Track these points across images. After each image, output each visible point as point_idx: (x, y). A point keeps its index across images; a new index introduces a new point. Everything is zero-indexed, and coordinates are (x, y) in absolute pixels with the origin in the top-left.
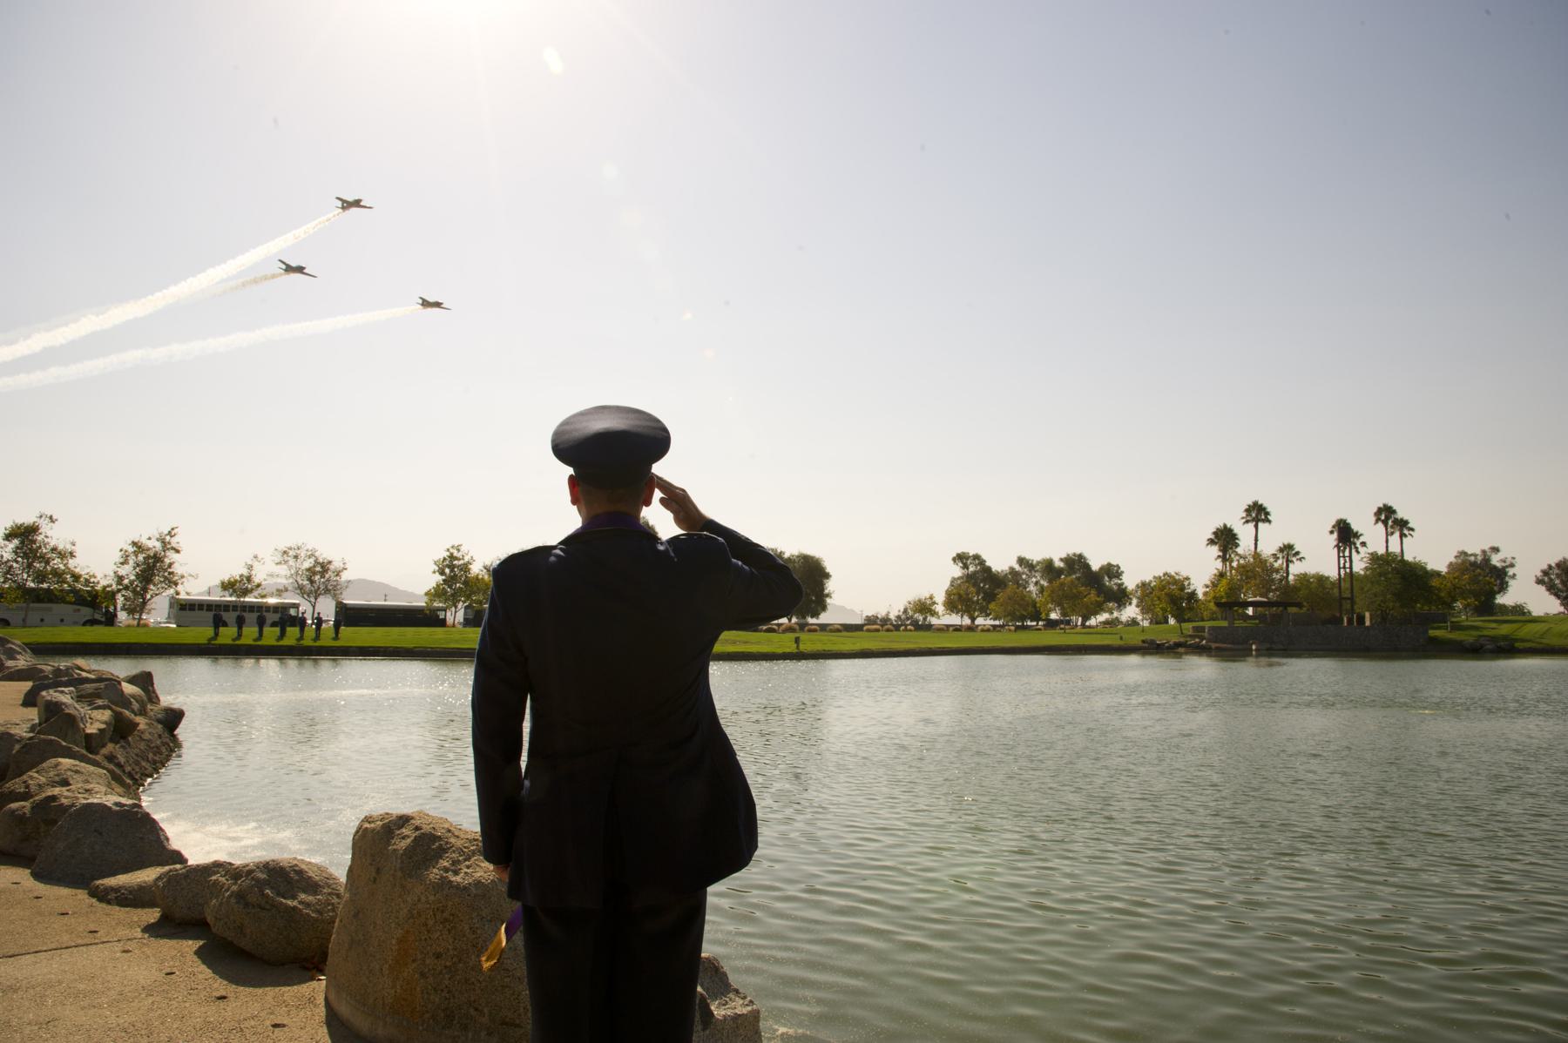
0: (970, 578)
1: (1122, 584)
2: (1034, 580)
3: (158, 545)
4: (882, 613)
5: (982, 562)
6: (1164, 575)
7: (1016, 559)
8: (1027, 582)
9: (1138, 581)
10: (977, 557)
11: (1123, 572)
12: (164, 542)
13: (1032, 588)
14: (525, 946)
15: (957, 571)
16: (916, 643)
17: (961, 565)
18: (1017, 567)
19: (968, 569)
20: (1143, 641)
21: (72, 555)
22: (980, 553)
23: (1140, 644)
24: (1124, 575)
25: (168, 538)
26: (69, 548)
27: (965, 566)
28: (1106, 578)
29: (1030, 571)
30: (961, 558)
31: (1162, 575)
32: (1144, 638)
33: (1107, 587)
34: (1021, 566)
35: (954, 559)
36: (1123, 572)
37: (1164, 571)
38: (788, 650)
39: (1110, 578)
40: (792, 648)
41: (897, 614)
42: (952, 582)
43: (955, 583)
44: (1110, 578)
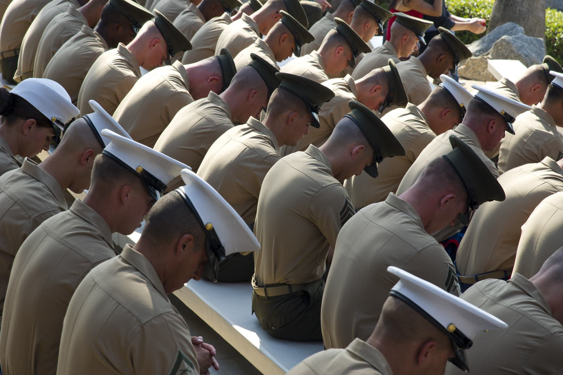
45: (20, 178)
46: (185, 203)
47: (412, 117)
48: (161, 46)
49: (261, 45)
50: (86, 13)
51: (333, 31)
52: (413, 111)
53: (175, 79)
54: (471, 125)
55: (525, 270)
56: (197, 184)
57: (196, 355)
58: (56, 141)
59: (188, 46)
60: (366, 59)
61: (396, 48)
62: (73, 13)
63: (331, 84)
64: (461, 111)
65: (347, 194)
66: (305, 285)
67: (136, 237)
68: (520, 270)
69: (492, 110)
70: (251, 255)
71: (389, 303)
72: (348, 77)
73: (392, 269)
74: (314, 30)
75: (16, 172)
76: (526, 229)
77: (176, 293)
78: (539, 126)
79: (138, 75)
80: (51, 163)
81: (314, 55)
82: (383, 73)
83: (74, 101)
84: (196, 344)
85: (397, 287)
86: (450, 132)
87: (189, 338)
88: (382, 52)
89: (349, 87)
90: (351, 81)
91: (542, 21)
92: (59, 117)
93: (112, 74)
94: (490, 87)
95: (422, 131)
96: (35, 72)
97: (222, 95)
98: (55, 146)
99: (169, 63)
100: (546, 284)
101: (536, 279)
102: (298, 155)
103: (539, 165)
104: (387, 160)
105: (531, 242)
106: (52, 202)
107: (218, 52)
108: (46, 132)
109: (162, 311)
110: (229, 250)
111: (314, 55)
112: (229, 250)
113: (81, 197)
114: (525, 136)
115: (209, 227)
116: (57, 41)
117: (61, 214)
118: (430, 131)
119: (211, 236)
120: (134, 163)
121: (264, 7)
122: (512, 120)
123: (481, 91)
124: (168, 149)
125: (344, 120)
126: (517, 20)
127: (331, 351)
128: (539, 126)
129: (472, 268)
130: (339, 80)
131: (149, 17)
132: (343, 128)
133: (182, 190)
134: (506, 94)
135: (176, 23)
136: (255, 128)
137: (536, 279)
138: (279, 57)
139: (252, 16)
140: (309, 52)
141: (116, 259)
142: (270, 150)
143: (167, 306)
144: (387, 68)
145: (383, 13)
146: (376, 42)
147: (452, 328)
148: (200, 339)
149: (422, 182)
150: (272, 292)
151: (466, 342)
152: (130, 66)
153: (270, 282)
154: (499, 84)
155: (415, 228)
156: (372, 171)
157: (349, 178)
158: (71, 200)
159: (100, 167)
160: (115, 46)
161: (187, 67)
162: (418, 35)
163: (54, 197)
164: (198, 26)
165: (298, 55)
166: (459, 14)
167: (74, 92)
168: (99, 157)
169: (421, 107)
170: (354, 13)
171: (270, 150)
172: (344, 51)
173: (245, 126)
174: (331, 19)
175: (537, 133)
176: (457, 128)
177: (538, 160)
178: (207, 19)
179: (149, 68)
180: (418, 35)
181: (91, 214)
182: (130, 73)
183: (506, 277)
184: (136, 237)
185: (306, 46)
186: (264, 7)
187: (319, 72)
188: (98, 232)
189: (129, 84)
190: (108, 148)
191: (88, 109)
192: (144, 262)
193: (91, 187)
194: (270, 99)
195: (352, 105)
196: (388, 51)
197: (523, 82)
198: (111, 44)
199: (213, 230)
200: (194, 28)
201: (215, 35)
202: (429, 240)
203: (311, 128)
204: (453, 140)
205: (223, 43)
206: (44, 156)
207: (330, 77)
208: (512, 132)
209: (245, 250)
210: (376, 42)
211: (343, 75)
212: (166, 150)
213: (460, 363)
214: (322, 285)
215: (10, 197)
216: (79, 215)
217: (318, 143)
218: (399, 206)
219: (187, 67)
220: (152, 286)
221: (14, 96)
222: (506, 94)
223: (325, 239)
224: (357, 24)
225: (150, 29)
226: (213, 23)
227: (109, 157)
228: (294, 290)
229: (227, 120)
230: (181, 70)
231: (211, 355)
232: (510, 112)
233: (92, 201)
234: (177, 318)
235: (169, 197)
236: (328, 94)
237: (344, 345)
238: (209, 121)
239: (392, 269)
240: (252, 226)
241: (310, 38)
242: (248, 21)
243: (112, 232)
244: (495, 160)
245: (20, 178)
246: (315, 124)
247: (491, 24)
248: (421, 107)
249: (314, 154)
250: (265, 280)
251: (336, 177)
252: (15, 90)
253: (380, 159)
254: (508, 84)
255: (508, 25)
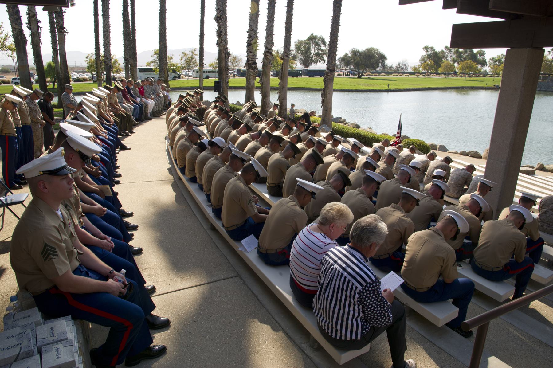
0: (429, 57)
1: (485, 58)
2: (450, 55)
3: (191, 53)
4: (275, 19)
5: (434, 50)
6: (502, 55)
7: (444, 47)
8: (447, 56)
9: (491, 57)
10: (432, 48)
11: (486, 53)
12: (193, 53)
13: (449, 58)
14: (28, 169)
15: (424, 53)
16: (420, 85)
17: (426, 50)
18: (444, 50)
19: (428, 52)
20: (494, 86)
21: (172, 58)
22: (433, 46)
23: (493, 86)
24: (486, 54)
25: (194, 51)
26: (171, 56)
27: (427, 51)
28: (479, 56)
29: (449, 52)
30: (426, 48)
31: (500, 55)
32: (494, 84)
33: (478, 59)
34: (446, 49)
35: (423, 48)
36: (486, 53)
37: (501, 53)
38: (386, 89)
39: (480, 56)
40: (386, 88)
41: (396, 65)
42: (422, 57)
43: (423, 58)
44: (480, 56)
45: (214, 160)
46: (251, 165)
47: (303, 145)
48: (246, 130)
49: (268, 129)
50: (228, 122)
51: (285, 125)
52: (303, 144)
53: (249, 137)
54: (317, 147)
55: (329, 179)
56: (254, 161)
57: (254, 199)
58: (222, 151)
59: (252, 130)
60: (292, 132)
61: (299, 130)
62: (226, 123)
63: (285, 137)
64: (314, 144)
65: (288, 163)
66: (279, 184)
67: (240, 173)
68: (327, 179)
69: (321, 144)
70: (266, 177)
71: (296, 187)
72: (288, 136)
73: (297, 179)
74: (281, 125)
75: (213, 158)
76: (329, 170)
77: (249, 186)
78: (331, 147)
79: (240, 136)
80: (221, 156)
81: (280, 131)
82: (296, 135)
83: (226, 142)
84: (254, 197)
85: (298, 183)
86: (312, 148)
87: (252, 196)
88: (296, 130)
89: (289, 138)
90: (289, 137)
91: (331, 125)
92: (222, 146)
93: (235, 136)
94: (320, 138)
95: (306, 148)
96: (218, 136)
97: (258, 140)
98: (222, 152)
99: (247, 133)
100: (333, 182)
101: (331, 181)
102: (277, 154)
103: (331, 156)
104: (297, 154)
105: (330, 173)
106: (221, 165)
107: (258, 130)
108: (220, 149)
109: (246, 189)
110: (261, 176)
111: (280, 131)
112: (261, 176)
113: (227, 164)
114: (328, 149)
115: (257, 171)
116: (222, 129)
117: (223, 168)
118: (307, 148)
119: (257, 172)
120: (239, 156)
121: (269, 120)
122: (326, 146)
123: (319, 139)
124: (247, 152)
125: (287, 145)
126: (326, 124)
127: (285, 198)
128: (331, 147)
129: (317, 179)
130: (286, 137)
131: (243, 123)
132: (288, 147)
133: (251, 162)
134: (324, 140)
135: (249, 124)
136: (267, 147)
137: (331, 181)
138: (273, 131)
139: (266, 122)
140: (279, 130)
141: (235, 177)
142: (270, 152)
143: (247, 188)
144: (297, 134)
145: (296, 122)
146: (295, 128)
147: (311, 191)
148: (255, 196)
149: (306, 160)
150: (271, 185)
151: (314, 194)
152: (238, 134)
153: (271, 183)
154: (322, 137)
155: (304, 170)
156: (294, 157)
157: (289, 159)
158: (225, 164)
159: (231, 157)
160: (235, 130)
161: (251, 134)
162: (304, 127)
163: (221, 164)
164: (254, 125)
165: (277, 131)
166: (313, 122)
167: (226, 140)
168: (231, 154)
169: (305, 143)
170: (289, 122)
171: (270, 152)
172: (287, 130)
173: (265, 147)
174: (284, 123)
175: (331, 149)
176: (313, 148)
177: (331, 155)
178: (256, 123)
179: (243, 134)
180: (304, 127)
181: (230, 167)
182: (239, 136)
183: (324, 180)
184: (240, 173)
185: (279, 129)
186: (269, 120)
187: (282, 135)
188: (231, 172)
189: (238, 138)
190: (233, 152)
191: (229, 144)
192: (242, 178)
193: (229, 161)
194: (180, 141)
195: (289, 142)
196: (297, 130)
197: (327, 137)
198: (234, 129)
199: (258, 171)
200: (253, 125)
201: (258, 127)
202: (307, 173)
203: (280, 147)
204: (313, 150)
205: (259, 129)
206: (219, 155)
207: (284, 136)
208: (326, 149)
209: (265, 176)
210: (295, 128)
211: (287, 136)
212: (246, 152)
213: (314, 198)
214: (283, 184)
215: (212, 164)
216: (227, 168)
217: (282, 151)
218: (300, 165)
219: (251, 134)
220: (244, 184)
221: (213, 141)
222: (324, 140)
223: (283, 173)
224: (290, 124)
225: (243, 126)
226: (257, 124)
227: (233, 154)
228: (277, 185)
229: (260, 145)
230: (250, 135)
231: (257, 199)
232: (325, 144)
233: (230, 165)
234: (250, 191)
235: (247, 163)
236: (284, 139)
237: (288, 197)
238: (256, 145)
239: (297, 179)
240: (266, 170)
241: (280, 127)
242: (265, 123)
243: (235, 171)
244: (322, 155)
245: (214, 160)
246: (281, 146)
247: (321, 124)
248: (305, 143)
249: (280, 153)
250: (270, 183)
251: (286, 159)
252: (213, 140)
253: (296, 154)
254: (324, 138)
255: (324, 125)
